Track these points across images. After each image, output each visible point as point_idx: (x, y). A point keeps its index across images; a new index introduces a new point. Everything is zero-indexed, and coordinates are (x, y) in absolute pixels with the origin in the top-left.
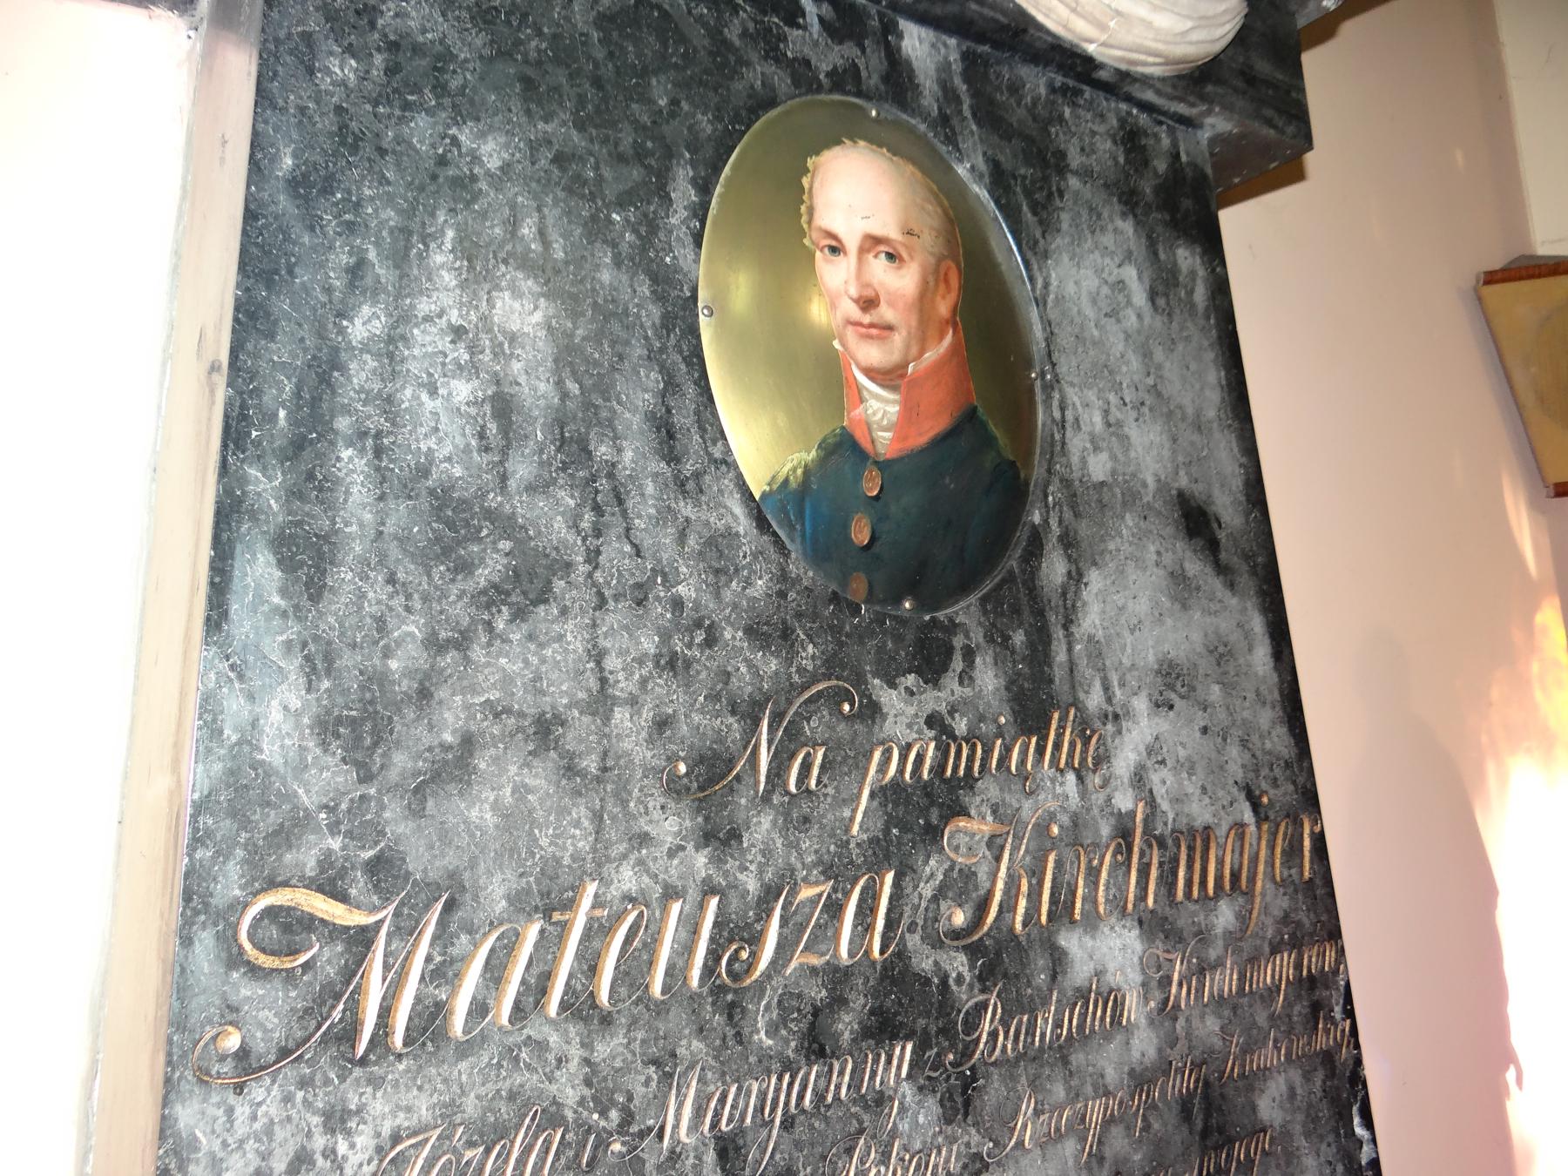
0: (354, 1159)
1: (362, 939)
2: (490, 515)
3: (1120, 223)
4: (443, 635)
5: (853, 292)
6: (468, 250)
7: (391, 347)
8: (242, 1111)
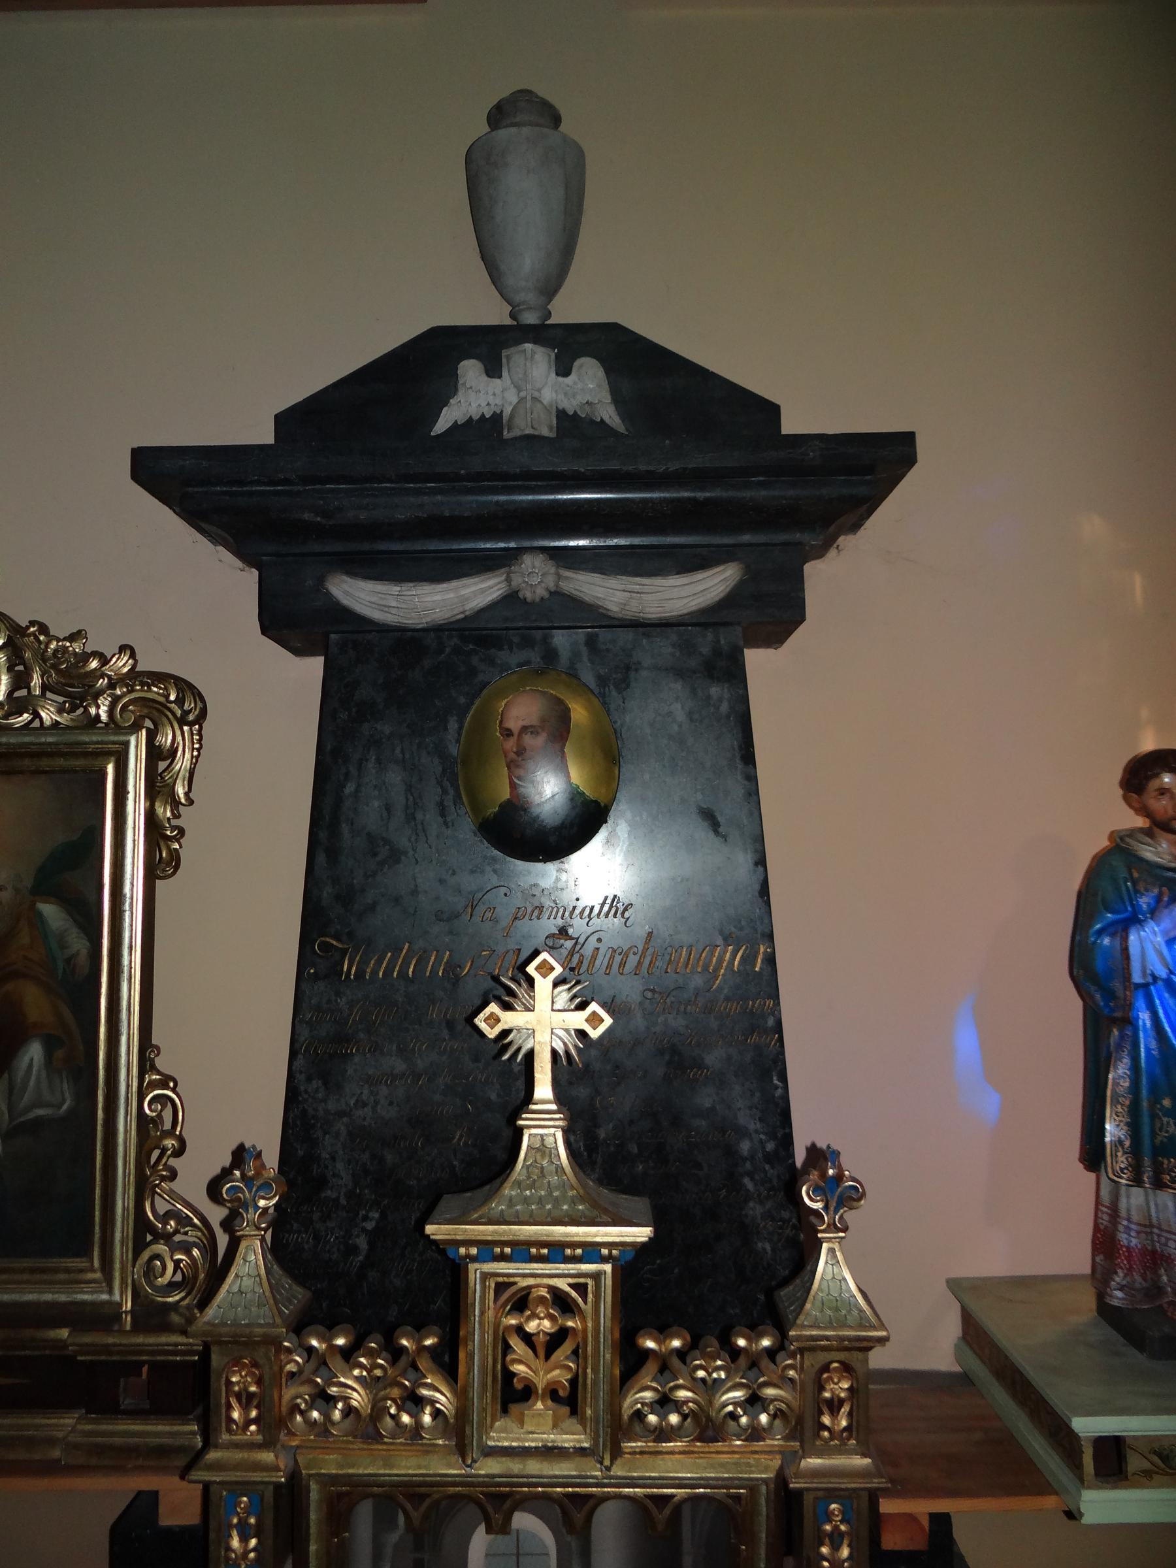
0: (341, 1004)
1: (344, 952)
2: (383, 839)
3: (672, 685)
4: (368, 874)
5: (515, 750)
6: (379, 761)
7: (356, 793)
8: (316, 987)
